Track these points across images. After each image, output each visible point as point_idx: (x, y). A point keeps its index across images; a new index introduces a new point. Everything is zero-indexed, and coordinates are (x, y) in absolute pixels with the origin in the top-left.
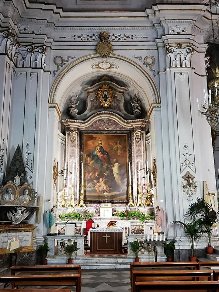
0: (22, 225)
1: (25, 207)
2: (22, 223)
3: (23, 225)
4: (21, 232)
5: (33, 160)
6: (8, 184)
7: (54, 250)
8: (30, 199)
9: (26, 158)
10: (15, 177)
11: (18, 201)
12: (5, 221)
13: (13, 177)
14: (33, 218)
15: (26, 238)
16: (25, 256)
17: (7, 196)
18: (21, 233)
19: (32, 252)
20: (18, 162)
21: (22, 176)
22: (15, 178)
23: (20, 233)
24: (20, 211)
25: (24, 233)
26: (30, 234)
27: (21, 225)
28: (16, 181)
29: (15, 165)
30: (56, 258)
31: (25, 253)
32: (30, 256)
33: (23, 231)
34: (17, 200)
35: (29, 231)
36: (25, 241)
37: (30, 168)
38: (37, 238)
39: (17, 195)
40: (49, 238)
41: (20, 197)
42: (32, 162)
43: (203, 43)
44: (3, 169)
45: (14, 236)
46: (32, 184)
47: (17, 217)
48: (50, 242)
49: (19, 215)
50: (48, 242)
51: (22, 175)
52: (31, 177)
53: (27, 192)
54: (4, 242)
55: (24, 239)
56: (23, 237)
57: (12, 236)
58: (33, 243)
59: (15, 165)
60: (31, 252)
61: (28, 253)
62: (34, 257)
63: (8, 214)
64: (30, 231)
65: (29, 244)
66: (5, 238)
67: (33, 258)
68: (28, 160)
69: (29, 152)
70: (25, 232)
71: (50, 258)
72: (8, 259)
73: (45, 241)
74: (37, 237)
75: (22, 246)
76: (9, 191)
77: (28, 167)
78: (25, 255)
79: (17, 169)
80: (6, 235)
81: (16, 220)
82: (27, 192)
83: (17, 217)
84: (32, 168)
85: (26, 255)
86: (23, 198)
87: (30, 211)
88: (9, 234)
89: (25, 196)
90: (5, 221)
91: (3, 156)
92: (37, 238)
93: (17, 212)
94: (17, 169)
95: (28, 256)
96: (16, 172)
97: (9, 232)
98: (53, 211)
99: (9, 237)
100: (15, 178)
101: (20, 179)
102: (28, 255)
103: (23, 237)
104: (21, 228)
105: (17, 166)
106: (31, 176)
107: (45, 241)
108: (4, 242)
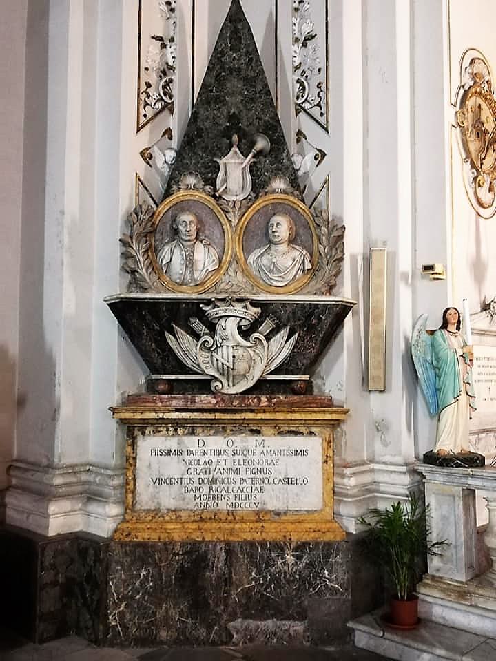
0: (264, 398)
1: (254, 304)
2: (261, 386)
3: (269, 400)
4: (258, 432)
5: (323, 66)
6: (179, 194)
7: (462, 552)
8: (308, 266)
9: (296, 68)
10: (224, 160)
11: (240, 276)
12: (173, 377)
13: (211, 161)
14: (336, 368)
15: (289, 466)
16: (285, 563)
17: (177, 252)
18: (259, 438)
19: (328, 544)
20: (234, 84)
21: (259, 153)
22: (221, 162)
23: (251, 441)
24: (230, 327)
25: (272, 441)
26: (314, 445)
27: (259, 400)
28: (225, 180)
29: (219, 100)
30: (475, 600)
31: (280, 548)
32: (311, 565)
33: (272, 431)
34: (231, 272)
35: (302, 429)
36: (286, 481)
37: (316, 112)
38: (377, 466)
39: (234, 247)
40: (436, 479)
41: (251, 259)
42: (321, 78)
43: (434, 606)
44: (175, 134)
45: (219, 452)
46: (328, 190)
47: (224, 356)
48: (438, 502)
49: (231, 343)
50: (431, 500)
51: (262, 143)
52: (321, 156)
53: (282, 227)
54: (161, 481)
55: (278, 472)
56: (270, 458)
57: (205, 453)
58: (336, 494)
59: (219, 100)
60: (317, 544)
61: (301, 548)
62: (342, 574)
63: (170, 338)
64: (311, 433)
65: (311, 498)
66: (166, 458)
67: (335, 577)
68: (304, 72)
69: (306, 29)
70: (280, 433)
71: (443, 591)
72: (182, 570)
73: (418, 496)
74: (377, 463)
75: (270, 507)
76: (180, 227)
77: (307, 106)
78: (282, 556)
79: (234, 119)
80: (172, 443)
81: (228, 372)
82: (282, 227)
83: (224, 356)
84: (324, 111)
85: (290, 558)
86: (265, 261)
87: (301, 327)
88: (191, 442)
89: (273, 247)
90: (173, 377)
91: (172, 68)
92: (377, 466)
93: (218, 329)
94: (234, 119)
95: (302, 565)
96: (227, 134)
97: (192, 433)
98: (452, 328)
99: (187, 458)
100: (221, 162)
101: (253, 167)
102: (299, 558)
103: (270, 458)
104: (250, 416)
105: (234, 103)
106: (320, 151)
107: (418, 496)
108: (161, 481)
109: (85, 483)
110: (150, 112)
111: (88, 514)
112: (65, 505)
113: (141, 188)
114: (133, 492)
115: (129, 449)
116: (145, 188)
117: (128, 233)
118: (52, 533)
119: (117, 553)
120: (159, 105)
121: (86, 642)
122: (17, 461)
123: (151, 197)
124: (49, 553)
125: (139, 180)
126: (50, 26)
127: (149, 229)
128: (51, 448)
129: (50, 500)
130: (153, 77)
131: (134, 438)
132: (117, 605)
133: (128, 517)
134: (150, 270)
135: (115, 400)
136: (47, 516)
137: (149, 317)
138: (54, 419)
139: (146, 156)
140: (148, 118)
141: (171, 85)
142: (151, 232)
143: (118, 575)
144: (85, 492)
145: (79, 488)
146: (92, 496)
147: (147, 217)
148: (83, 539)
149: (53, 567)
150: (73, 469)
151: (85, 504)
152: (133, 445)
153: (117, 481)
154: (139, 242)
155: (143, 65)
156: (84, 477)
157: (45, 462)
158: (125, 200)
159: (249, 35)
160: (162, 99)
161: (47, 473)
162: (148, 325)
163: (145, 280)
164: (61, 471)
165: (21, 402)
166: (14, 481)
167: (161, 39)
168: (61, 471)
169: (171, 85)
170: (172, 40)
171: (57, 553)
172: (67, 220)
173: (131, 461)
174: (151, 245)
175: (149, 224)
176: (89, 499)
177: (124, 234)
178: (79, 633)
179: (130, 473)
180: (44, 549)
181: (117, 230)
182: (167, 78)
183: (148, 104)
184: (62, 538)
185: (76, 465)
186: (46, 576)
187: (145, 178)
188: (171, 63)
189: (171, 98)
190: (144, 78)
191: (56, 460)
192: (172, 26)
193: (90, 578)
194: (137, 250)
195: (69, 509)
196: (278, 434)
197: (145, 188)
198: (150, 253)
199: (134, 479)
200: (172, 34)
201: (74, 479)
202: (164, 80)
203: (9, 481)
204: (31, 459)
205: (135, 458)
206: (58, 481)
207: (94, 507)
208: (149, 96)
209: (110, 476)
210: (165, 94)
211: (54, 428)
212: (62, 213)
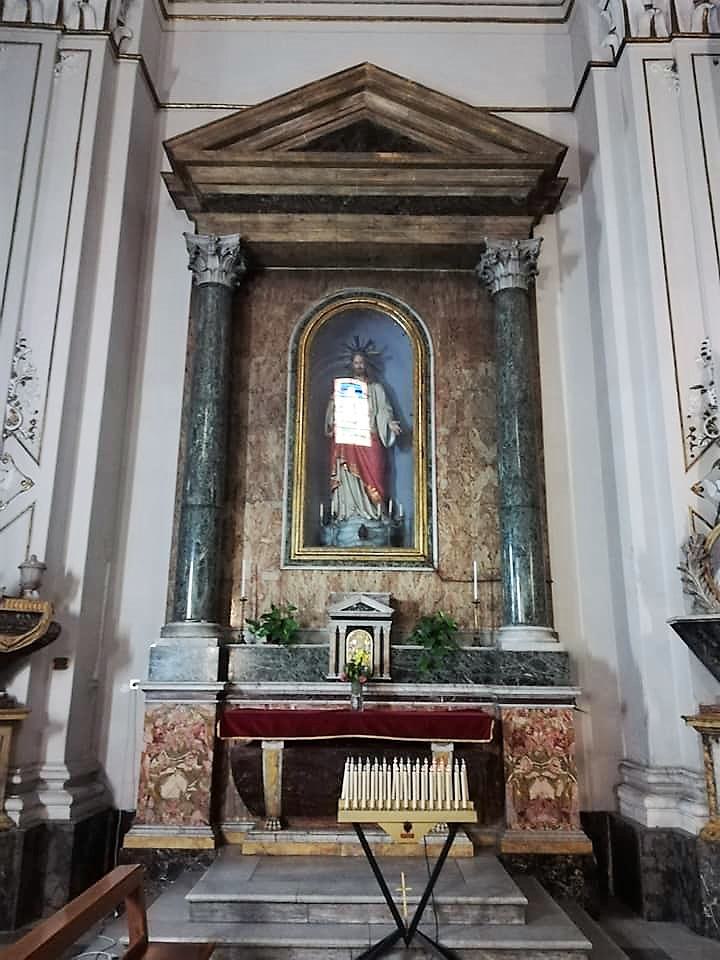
91: (715, 407)
109: (679, 785)
110: (697, 451)
111: (682, 813)
112: (660, 801)
113: (696, 517)
114: (715, 795)
115: (707, 755)
116: (700, 517)
117: (685, 562)
118: (651, 824)
119: (704, 850)
120: (705, 443)
121: (688, 929)
122: (627, 760)
123: (708, 524)
124: (648, 840)
125: (693, 512)
126: (611, 402)
127: (702, 556)
128: (647, 753)
129: (647, 795)
130: (697, 422)
131: (709, 745)
132: (710, 900)
133: (714, 819)
134: (708, 591)
135: (693, 710)
136: (645, 810)
137: (705, 636)
138: (646, 724)
139: (699, 490)
140: (696, 456)
141: (715, 422)
142: (704, 558)
143: (707, 870)
144: (681, 793)
145: (675, 789)
146: (685, 797)
147: (698, 546)
148: (678, 834)
149: (653, 854)
150: (667, 771)
151: (678, 803)
152: (709, 751)
153: (702, 785)
154: (694, 568)
155: (685, 415)
156: (677, 779)
157: (644, 762)
158: (681, 531)
159: (525, 350)
160: (708, 437)
161: (644, 771)
162: (706, 642)
163: (704, 602)
164: (655, 771)
165: (624, 710)
166: (626, 779)
167: (700, 387)
168: (655, 771)
169: (715, 422)
170: (712, 383)
171: (655, 843)
172: (636, 554)
173: (709, 766)
174: (706, 569)
175: (702, 551)
176: (682, 799)
177: (681, 563)
178: (683, 921)
179: (709, 777)
180: (642, 838)
181: (678, 558)
182: (710, 418)
183: (693, 446)
184: (658, 831)
185: (671, 768)
186: (647, 861)
187: (699, 510)
188: (713, 404)
189: (716, 433)
190: (687, 424)
191: (651, 761)
192: (710, 371)
193: (685, 870)
194: (694, 574)
195: (663, 806)
196: (574, 699)
197: (700, 517)
198: (706, 576)
199: (714, 783)
200: (711, 379)
201: (667, 780)
202: (707, 421)
203: (622, 778)
204: (636, 759)
205: (712, 764)
206: (652, 779)
207: (684, 806)
208: (694, 438)
209: (695, 779)
210: (710, 432)
211: (646, 732)
212: (632, 549)
